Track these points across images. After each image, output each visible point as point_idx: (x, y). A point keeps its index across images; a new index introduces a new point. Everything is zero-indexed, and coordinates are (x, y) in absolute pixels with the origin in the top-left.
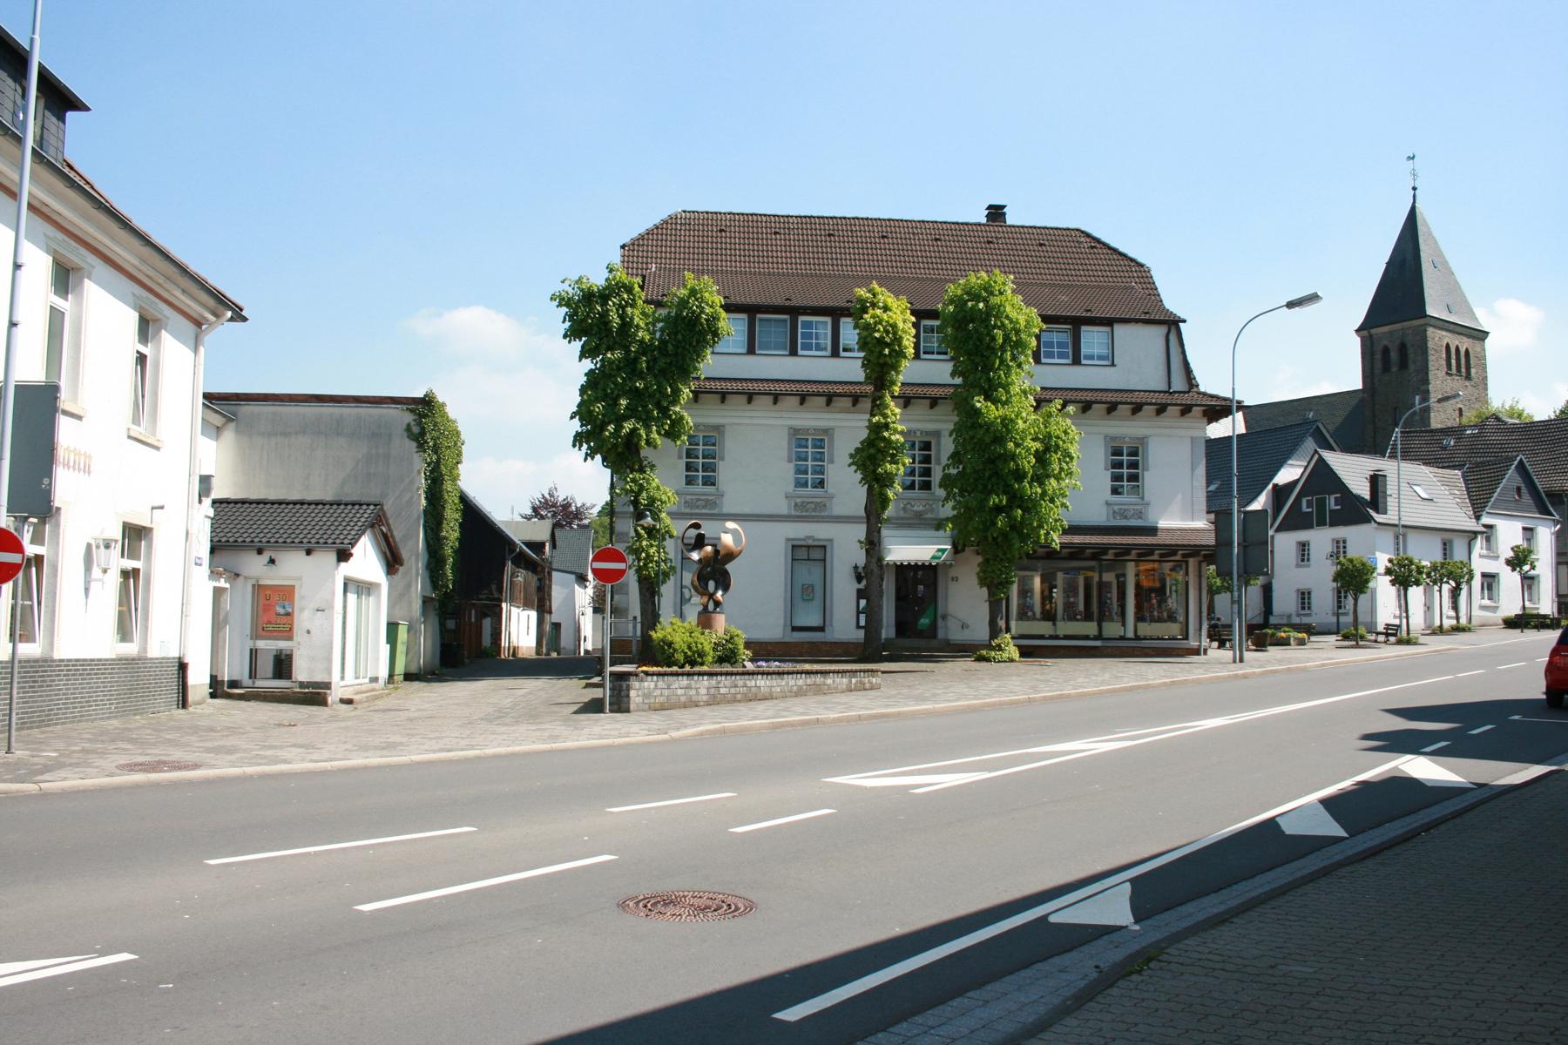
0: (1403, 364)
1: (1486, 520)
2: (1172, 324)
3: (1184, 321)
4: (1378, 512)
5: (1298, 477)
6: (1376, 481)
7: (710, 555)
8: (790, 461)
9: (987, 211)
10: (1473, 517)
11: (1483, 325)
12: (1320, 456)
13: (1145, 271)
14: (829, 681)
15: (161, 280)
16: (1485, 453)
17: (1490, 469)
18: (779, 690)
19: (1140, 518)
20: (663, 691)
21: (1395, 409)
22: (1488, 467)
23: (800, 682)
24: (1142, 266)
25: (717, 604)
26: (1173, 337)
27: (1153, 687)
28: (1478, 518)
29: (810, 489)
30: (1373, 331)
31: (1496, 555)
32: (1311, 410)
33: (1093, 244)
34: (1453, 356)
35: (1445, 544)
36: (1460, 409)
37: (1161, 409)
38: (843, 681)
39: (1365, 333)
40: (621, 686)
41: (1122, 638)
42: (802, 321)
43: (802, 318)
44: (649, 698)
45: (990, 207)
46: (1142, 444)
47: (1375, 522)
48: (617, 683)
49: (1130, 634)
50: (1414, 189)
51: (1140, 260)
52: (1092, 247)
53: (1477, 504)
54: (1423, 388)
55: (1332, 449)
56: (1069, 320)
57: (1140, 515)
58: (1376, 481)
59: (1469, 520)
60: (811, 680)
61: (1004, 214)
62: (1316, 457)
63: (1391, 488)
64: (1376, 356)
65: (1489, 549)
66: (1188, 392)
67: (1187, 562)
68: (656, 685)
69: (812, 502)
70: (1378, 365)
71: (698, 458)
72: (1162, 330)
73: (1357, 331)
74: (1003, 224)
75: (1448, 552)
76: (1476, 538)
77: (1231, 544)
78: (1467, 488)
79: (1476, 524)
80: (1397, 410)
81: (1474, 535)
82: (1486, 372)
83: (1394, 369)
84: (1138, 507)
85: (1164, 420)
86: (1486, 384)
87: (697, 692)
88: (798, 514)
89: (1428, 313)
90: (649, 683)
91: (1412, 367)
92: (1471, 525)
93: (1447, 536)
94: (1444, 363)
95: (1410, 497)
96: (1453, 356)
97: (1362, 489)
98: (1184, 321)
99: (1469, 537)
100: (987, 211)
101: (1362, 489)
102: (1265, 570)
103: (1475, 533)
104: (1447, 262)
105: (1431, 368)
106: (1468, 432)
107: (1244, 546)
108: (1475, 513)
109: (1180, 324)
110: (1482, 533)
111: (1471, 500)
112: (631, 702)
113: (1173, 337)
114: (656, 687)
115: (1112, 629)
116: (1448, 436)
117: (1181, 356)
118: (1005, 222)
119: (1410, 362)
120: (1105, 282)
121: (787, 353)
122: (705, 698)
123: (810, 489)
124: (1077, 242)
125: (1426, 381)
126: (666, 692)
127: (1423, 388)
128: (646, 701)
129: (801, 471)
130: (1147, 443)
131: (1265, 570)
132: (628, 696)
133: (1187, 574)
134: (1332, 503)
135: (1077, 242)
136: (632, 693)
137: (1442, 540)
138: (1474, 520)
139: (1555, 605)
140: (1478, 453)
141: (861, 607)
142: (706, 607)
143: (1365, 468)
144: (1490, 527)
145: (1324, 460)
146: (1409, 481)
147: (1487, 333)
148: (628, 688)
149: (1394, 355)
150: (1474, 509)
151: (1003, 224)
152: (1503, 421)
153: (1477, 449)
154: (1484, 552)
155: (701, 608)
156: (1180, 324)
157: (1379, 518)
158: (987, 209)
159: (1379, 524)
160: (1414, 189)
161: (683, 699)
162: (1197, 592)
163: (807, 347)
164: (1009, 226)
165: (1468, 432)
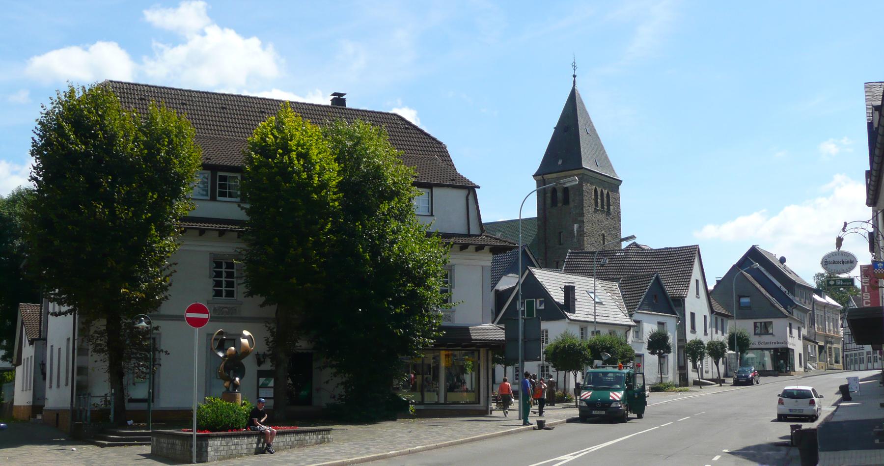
0: (566, 201)
1: (637, 317)
2: (470, 189)
3: (479, 187)
4: (570, 312)
5: (514, 285)
6: (569, 291)
7: (233, 353)
8: (210, 277)
9: (333, 97)
10: (628, 315)
11: (618, 176)
12: (530, 271)
13: (442, 148)
14: (307, 438)
15: (586, 316)
16: (629, 269)
17: (637, 282)
18: (282, 444)
19: (449, 320)
20: (225, 447)
21: (560, 233)
22: (636, 281)
23: (293, 439)
24: (440, 143)
25: (236, 386)
26: (471, 198)
27: (165, 434)
28: (631, 316)
29: (224, 298)
30: (546, 177)
31: (642, 341)
32: (499, 231)
33: (406, 126)
34: (599, 197)
35: (582, 329)
36: (603, 234)
37: (463, 247)
38: (314, 437)
39: (540, 177)
40: (202, 444)
41: (437, 403)
42: (219, 176)
43: (220, 173)
44: (217, 452)
45: (335, 94)
46: (451, 270)
47: (568, 318)
48: (199, 442)
49: (442, 401)
50: (574, 76)
51: (439, 139)
52: (406, 128)
53: (630, 306)
54: (579, 219)
55: (534, 266)
56: (836, 330)
57: (449, 318)
58: (569, 291)
59: (625, 317)
60: (298, 437)
61: (344, 100)
62: (527, 272)
63: (578, 295)
64: (547, 195)
65: (637, 337)
66: (480, 235)
67: (479, 352)
68: (221, 443)
69: (226, 308)
70: (549, 201)
71: (225, 290)
72: (463, 193)
73: (534, 176)
74: (344, 107)
75: (584, 336)
76: (630, 329)
77: (517, 340)
78: (623, 295)
79: (630, 320)
80: (562, 234)
81: (629, 328)
82: (620, 209)
83: (560, 205)
84: (448, 313)
85: (465, 254)
86: (620, 218)
87: (241, 447)
88: (216, 316)
89: (583, 166)
90: (217, 442)
91: (572, 205)
92: (628, 321)
93: (612, 328)
94: (593, 201)
95: (557, 291)
96: (599, 197)
97: (559, 297)
98: (479, 187)
99: (625, 329)
100: (333, 97)
101: (559, 297)
102: (538, 357)
103: (630, 326)
104: (595, 130)
105: (585, 205)
106: (617, 254)
107: (525, 341)
108: (629, 312)
109: (476, 189)
110: (634, 326)
111: (626, 303)
112: (209, 455)
113: (471, 198)
114: (221, 445)
115: (430, 398)
116: (605, 256)
117: (477, 211)
118: (345, 106)
119: (571, 200)
120: (411, 153)
121: (208, 198)
122: (245, 451)
123: (224, 298)
124: (396, 123)
125: (582, 215)
126: (226, 448)
127: (579, 219)
128: (216, 454)
129: (218, 284)
130: (454, 270)
131: (538, 357)
132: (206, 451)
133: (479, 359)
134: (539, 305)
135: (396, 123)
136: (209, 449)
137: (609, 331)
138: (628, 317)
139: (677, 376)
140: (625, 269)
141: (260, 383)
142: (227, 388)
143: (583, 289)
144: (637, 322)
145: (533, 275)
146: (587, 290)
147: (621, 181)
148: (207, 446)
149: (560, 195)
150: (628, 309)
151: (344, 107)
152: (641, 248)
153: (624, 266)
154: (636, 340)
155: (224, 390)
156: (476, 189)
157: (571, 316)
158: (332, 95)
159: (571, 320)
160: (574, 76)
161: (234, 452)
162: (486, 371)
163: (223, 194)
164: (349, 109)
165: (617, 254)
